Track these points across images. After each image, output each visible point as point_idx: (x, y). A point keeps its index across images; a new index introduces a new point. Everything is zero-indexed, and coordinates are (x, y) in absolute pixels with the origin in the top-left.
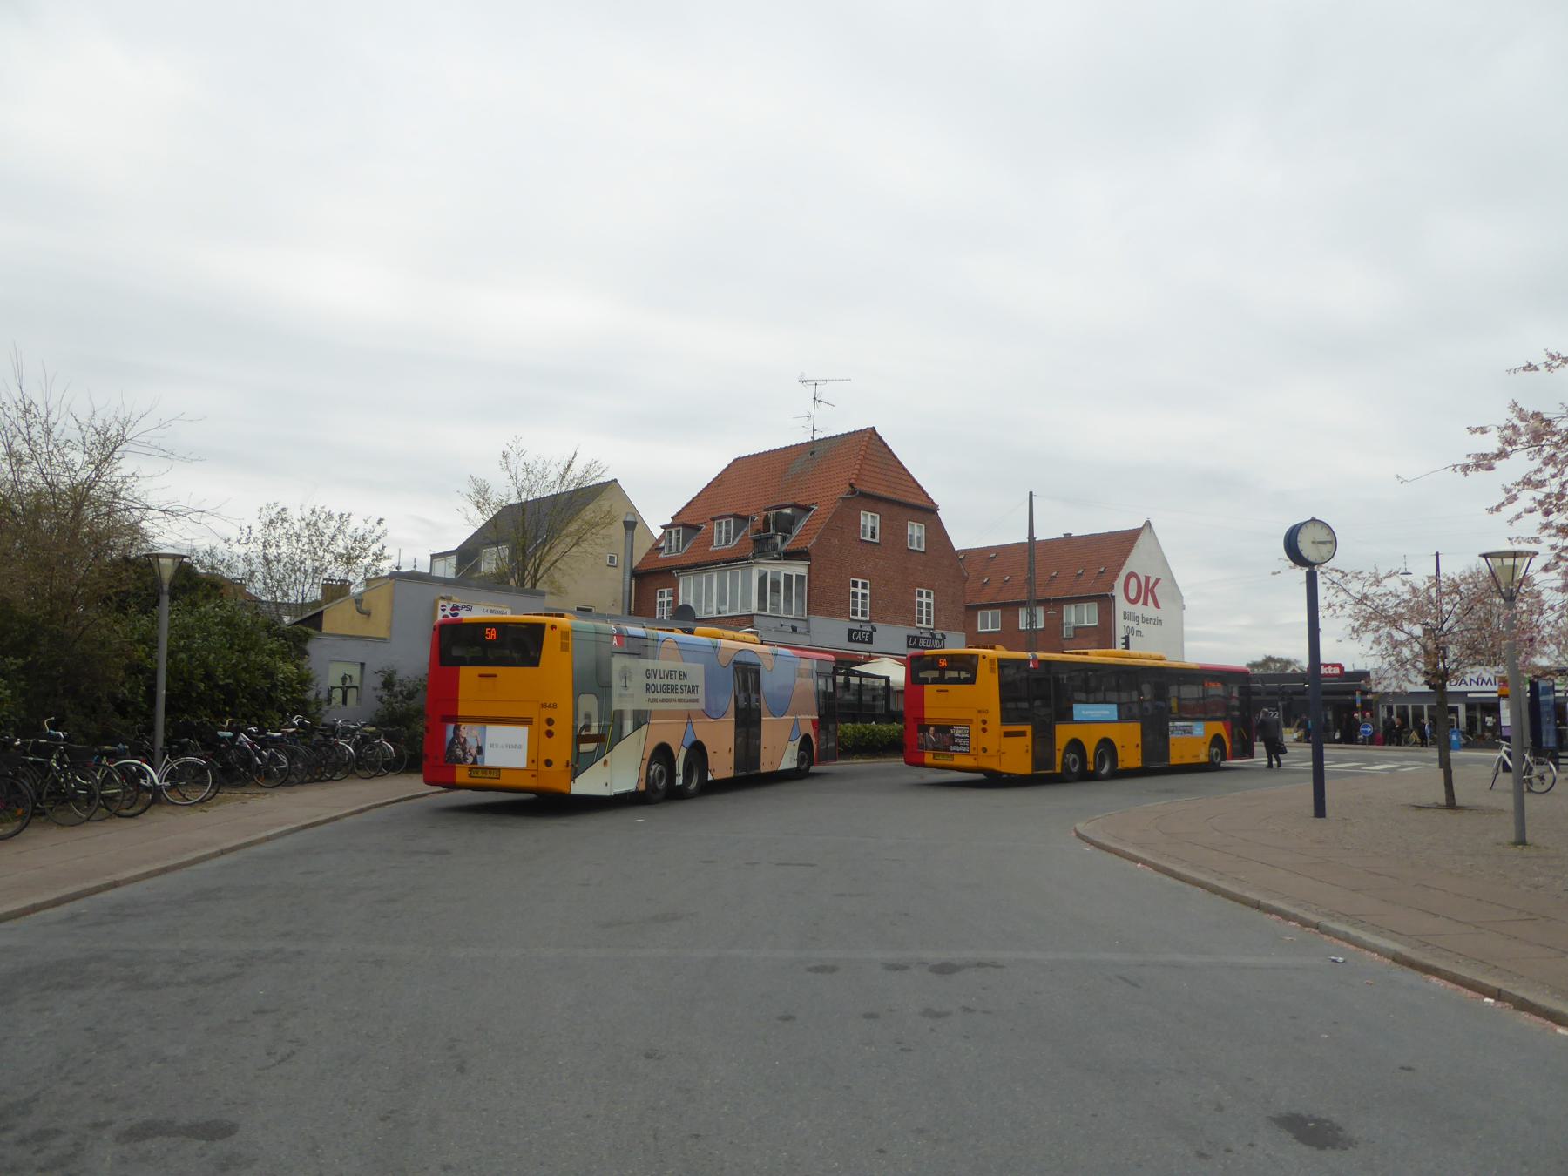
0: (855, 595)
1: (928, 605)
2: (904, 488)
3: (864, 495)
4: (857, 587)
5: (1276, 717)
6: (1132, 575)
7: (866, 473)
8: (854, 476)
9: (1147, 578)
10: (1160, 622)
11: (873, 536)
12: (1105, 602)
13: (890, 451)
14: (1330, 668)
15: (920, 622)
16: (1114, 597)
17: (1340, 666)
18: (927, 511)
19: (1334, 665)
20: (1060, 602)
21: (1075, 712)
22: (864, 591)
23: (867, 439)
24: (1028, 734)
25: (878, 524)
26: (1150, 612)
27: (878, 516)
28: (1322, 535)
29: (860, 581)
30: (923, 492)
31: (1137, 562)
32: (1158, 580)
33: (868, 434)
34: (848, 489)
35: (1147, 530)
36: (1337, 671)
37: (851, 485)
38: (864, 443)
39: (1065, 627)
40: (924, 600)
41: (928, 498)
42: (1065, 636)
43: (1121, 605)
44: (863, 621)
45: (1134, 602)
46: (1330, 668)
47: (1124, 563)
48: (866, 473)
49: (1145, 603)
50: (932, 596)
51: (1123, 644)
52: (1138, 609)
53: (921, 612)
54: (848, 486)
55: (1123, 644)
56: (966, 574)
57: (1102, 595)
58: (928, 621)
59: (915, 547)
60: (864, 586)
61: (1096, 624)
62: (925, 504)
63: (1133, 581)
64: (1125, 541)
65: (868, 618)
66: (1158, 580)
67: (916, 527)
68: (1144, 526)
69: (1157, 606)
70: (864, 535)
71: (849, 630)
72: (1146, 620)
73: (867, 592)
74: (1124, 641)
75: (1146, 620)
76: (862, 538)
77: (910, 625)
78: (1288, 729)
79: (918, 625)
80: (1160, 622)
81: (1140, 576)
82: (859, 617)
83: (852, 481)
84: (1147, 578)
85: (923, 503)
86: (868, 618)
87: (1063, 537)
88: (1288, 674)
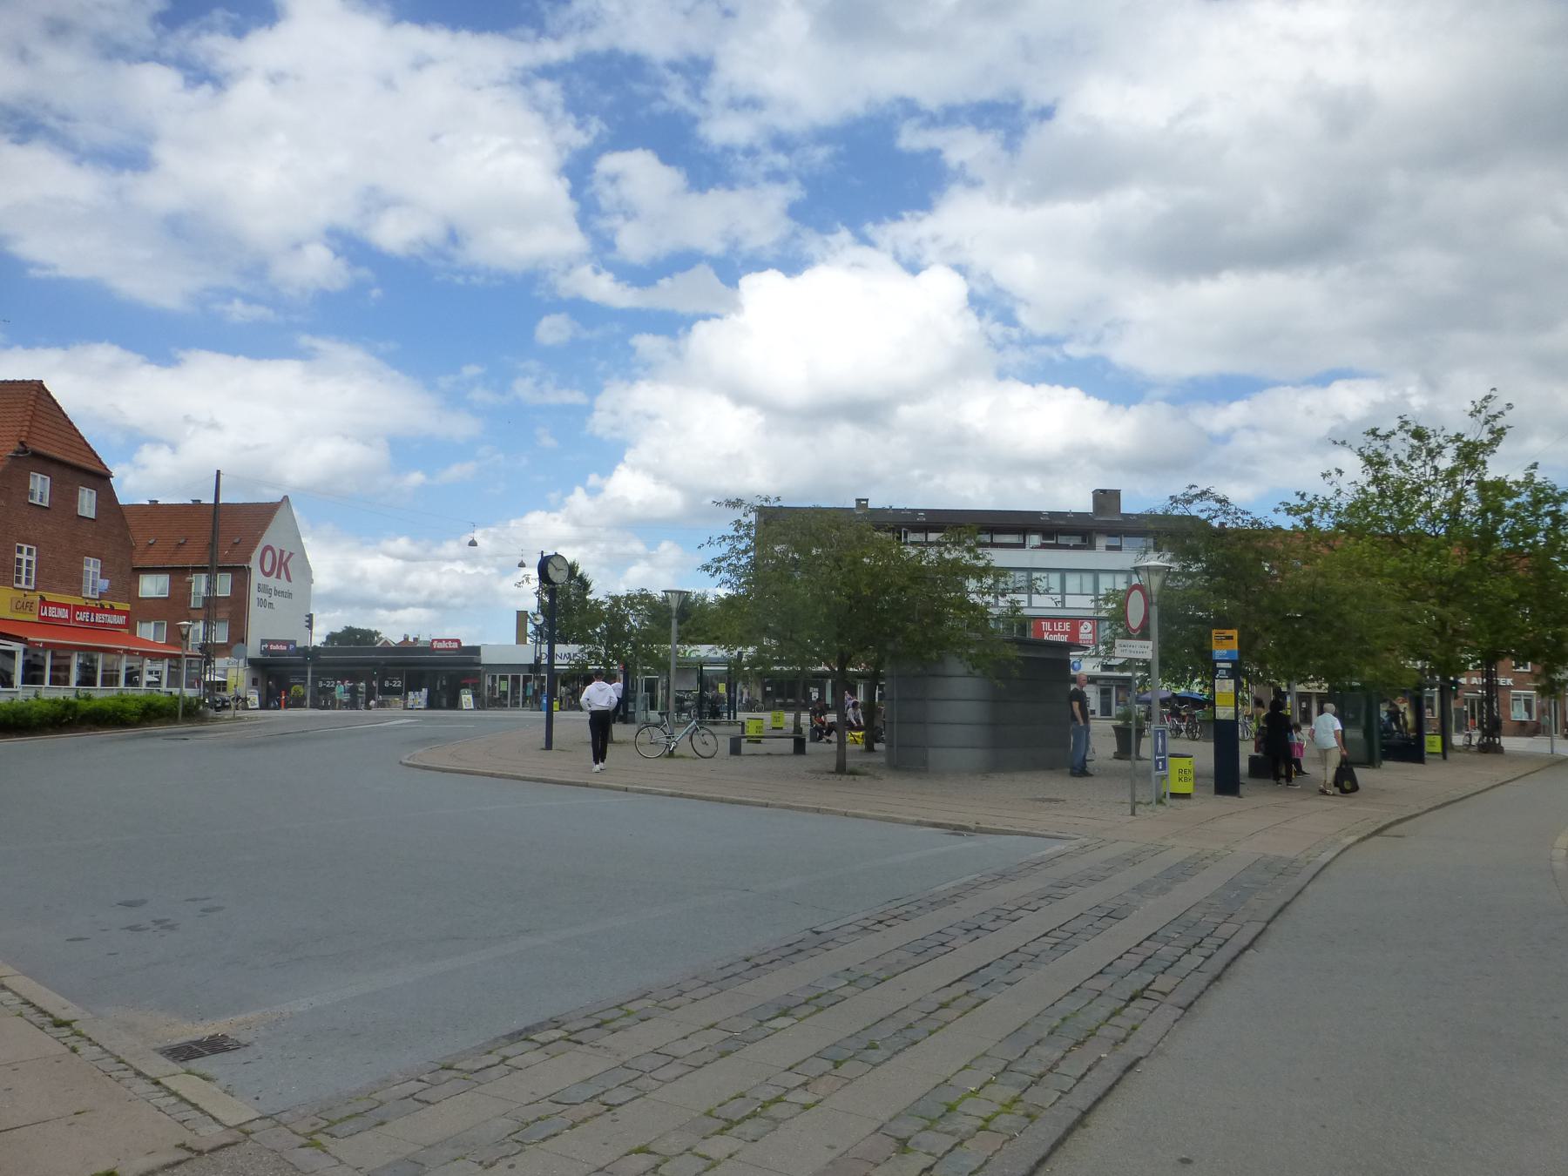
0: (19, 561)
1: (29, 563)
2: (76, 450)
3: (37, 455)
4: (89, 565)
5: (399, 685)
6: (268, 548)
7: (38, 431)
8: (25, 434)
9: (282, 552)
10: (290, 595)
11: (41, 500)
12: (240, 573)
13: (54, 401)
14: (450, 643)
15: (18, 580)
16: (250, 569)
17: (458, 641)
18: (100, 478)
19: (453, 641)
20: (185, 570)
21: (1362, 734)
22: (29, 558)
23: (34, 393)
24: (1096, 712)
25: (48, 490)
26: (282, 584)
27: (49, 478)
28: (1400, 446)
29: (25, 547)
30: (96, 456)
31: (272, 536)
32: (291, 554)
33: (36, 388)
34: (16, 446)
35: (284, 505)
36: (455, 645)
37: (22, 443)
38: (32, 397)
39: (193, 596)
40: (24, 557)
41: (101, 462)
42: (192, 606)
43: (256, 577)
44: (28, 590)
45: (268, 575)
46: (450, 643)
47: (261, 535)
48: (38, 431)
49: (278, 577)
50: (35, 553)
51: (307, 621)
52: (272, 582)
53: (19, 571)
54: (17, 443)
55: (307, 621)
56: (134, 544)
57: (240, 567)
58: (28, 581)
59: (37, 502)
60: (29, 552)
61: (167, 596)
62: (98, 469)
63: (269, 554)
64: (262, 514)
65: (32, 587)
66: (291, 554)
67: (39, 479)
68: (282, 500)
69: (289, 579)
70: (32, 498)
71: (295, 641)
72: (277, 593)
73: (33, 558)
74: (308, 618)
75: (277, 593)
76: (31, 501)
77: (76, 595)
78: (1523, 720)
79: (16, 585)
80: (290, 595)
81: (275, 549)
82: (23, 585)
83: (23, 439)
84: (282, 552)
85: (94, 467)
86: (32, 587)
87: (191, 502)
88: (378, 647)
